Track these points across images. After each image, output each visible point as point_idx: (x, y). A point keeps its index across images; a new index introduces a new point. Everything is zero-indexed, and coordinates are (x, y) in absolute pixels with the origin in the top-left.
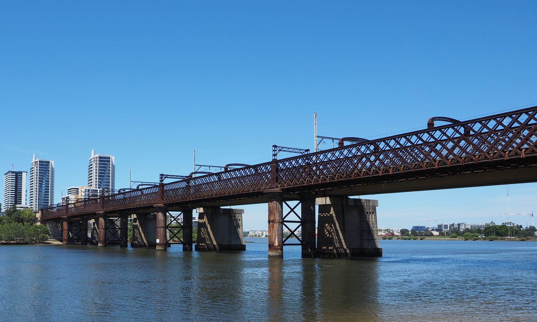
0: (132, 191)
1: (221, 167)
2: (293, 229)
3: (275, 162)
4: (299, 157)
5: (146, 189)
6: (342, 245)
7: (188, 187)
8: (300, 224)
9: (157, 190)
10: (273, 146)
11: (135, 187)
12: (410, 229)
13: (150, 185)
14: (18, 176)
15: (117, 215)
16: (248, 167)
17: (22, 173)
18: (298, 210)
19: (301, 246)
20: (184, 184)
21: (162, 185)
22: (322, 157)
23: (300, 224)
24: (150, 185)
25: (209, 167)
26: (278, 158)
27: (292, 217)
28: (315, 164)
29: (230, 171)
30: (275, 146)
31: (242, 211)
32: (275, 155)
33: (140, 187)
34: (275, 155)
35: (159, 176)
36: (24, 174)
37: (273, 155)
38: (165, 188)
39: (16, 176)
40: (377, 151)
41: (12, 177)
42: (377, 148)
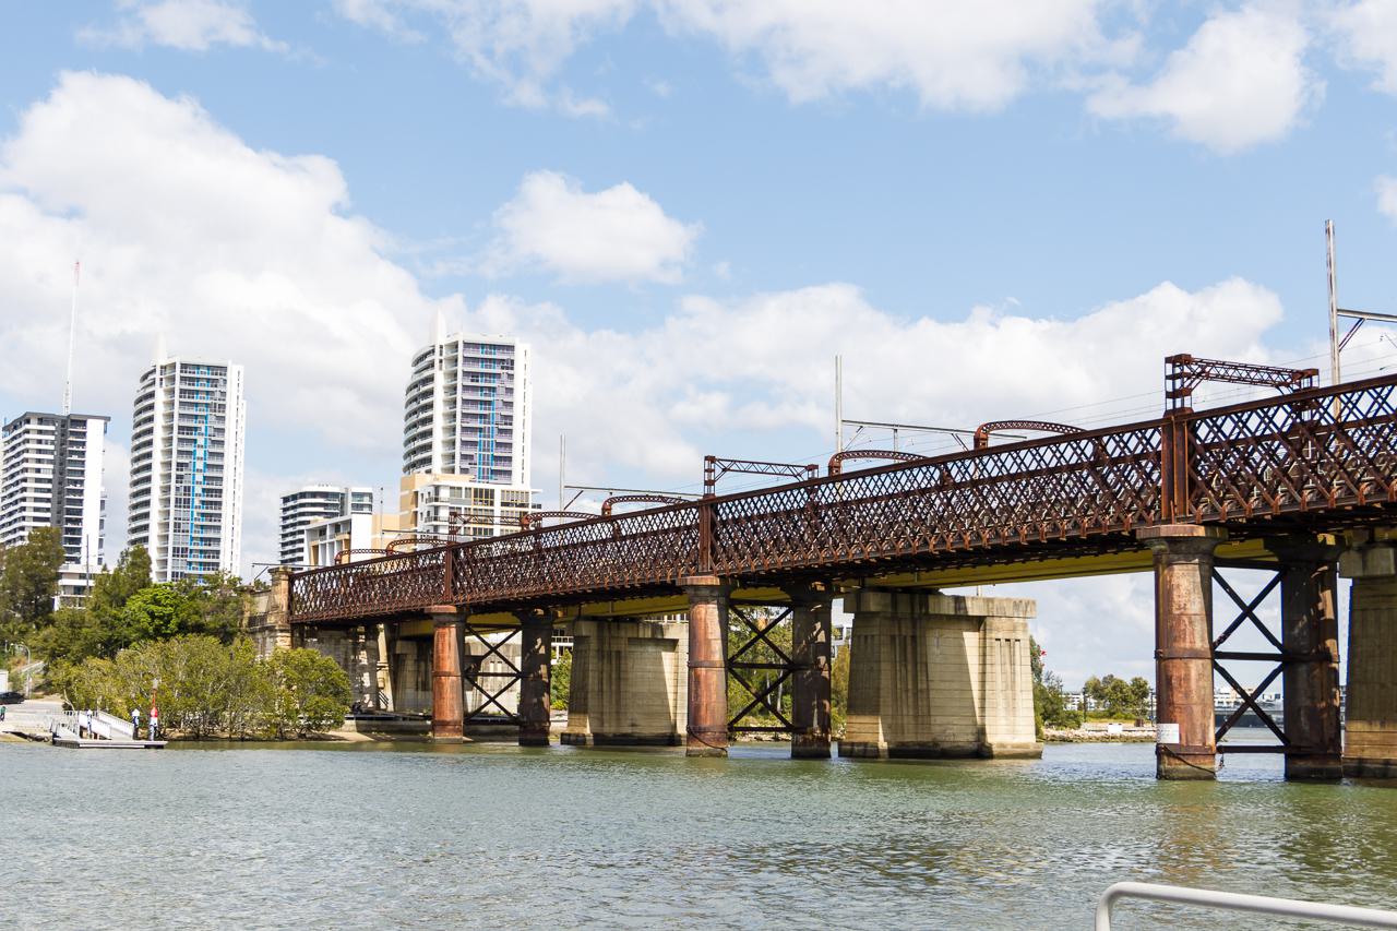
0: (583, 524)
1: (955, 433)
2: (1250, 686)
3: (710, 504)
4: (1278, 402)
5: (633, 515)
6: (776, 705)
7: (1301, 434)
8: (1277, 664)
9: (690, 517)
10: (706, 458)
11: (596, 509)
12: (1101, 679)
13: (647, 498)
14: (70, 430)
15: (507, 618)
16: (1074, 436)
17: (84, 423)
18: (1271, 612)
19: (1281, 757)
20: (800, 499)
21: (1179, 422)
22: (1254, 422)
23: (1277, 664)
24: (647, 498)
25: (895, 428)
26: (721, 489)
27: (1247, 638)
28: (1340, 427)
29: (999, 450)
30: (711, 459)
31: (1024, 607)
32: (709, 483)
33: (617, 509)
34: (709, 483)
35: (701, 465)
36: (94, 429)
37: (1169, 395)
38: (724, 513)
39: (62, 441)
40: (945, 484)
41: (40, 444)
42: (1100, 450)
